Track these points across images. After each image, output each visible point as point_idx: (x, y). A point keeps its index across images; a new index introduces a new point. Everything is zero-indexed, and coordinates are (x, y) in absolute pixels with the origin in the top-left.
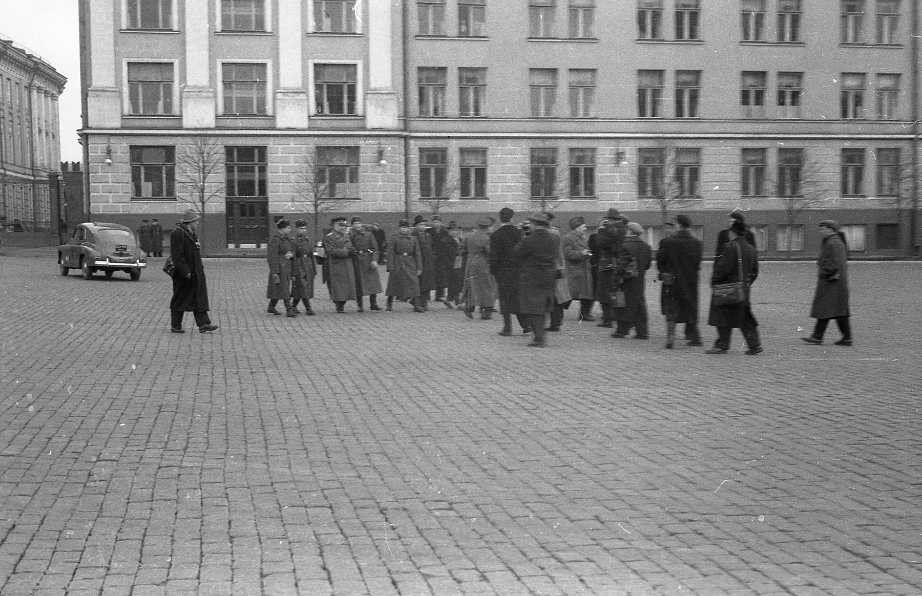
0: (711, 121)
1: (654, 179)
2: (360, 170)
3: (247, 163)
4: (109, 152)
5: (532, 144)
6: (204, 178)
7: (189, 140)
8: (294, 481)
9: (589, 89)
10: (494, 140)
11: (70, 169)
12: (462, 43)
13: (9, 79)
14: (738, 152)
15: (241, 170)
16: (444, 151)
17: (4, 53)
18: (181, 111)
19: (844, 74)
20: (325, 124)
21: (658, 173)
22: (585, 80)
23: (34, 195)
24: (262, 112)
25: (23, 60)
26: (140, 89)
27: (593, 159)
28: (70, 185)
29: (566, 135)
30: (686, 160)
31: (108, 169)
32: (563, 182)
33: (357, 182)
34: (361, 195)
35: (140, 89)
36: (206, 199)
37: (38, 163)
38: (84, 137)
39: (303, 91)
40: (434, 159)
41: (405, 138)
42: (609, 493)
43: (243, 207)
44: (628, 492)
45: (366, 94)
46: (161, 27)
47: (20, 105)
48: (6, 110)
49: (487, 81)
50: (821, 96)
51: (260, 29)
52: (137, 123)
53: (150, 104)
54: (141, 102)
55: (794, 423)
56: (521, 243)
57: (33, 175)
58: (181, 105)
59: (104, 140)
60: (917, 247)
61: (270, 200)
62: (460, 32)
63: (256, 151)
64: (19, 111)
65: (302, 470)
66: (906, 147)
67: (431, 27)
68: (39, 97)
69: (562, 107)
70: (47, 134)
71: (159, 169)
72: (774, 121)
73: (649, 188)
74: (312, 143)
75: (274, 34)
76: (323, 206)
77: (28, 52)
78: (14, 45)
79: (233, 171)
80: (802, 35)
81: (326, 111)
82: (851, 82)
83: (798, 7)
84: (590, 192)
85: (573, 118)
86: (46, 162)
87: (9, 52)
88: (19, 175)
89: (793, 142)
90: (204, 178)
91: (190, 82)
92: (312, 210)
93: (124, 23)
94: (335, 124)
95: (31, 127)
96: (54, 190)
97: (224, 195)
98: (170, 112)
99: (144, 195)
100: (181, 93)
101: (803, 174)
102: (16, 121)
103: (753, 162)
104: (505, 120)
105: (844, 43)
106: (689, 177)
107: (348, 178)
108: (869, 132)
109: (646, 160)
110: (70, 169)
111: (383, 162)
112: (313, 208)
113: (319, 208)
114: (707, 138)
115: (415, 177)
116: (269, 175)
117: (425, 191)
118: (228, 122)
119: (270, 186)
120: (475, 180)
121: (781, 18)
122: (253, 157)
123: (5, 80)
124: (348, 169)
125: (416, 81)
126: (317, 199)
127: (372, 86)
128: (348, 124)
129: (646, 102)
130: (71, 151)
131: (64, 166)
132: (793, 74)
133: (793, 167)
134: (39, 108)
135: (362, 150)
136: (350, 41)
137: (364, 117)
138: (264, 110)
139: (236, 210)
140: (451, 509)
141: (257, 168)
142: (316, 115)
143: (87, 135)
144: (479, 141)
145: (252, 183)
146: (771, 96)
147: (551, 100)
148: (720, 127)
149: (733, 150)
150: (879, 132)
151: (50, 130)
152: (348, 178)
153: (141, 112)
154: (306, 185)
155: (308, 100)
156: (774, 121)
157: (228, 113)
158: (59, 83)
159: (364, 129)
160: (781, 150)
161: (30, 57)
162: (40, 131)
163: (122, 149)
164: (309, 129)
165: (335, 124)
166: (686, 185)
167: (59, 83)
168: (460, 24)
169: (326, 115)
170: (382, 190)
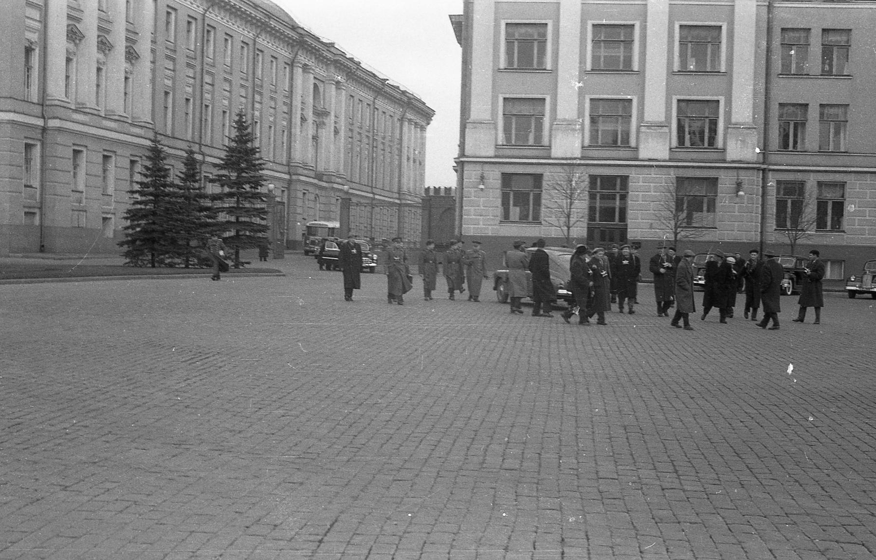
7: (559, 169)
11: (432, 194)
12: (825, 82)
13: (384, 113)
15: (603, 197)
16: (802, 184)
18: (550, 141)
23: (399, 219)
25: (398, 96)
26: (514, 121)
28: (441, 206)
34: (717, 224)
35: (514, 121)
36: (571, 223)
37: (405, 189)
38: (460, 166)
39: (666, 125)
41: (764, 170)
43: (603, 233)
45: (726, 128)
46: (535, 66)
51: (627, 68)
52: (508, 152)
54: (513, 132)
58: (550, 136)
61: (629, 226)
62: (823, 70)
63: (619, 181)
67: (794, 66)
68: (410, 130)
70: (414, 161)
74: (673, 173)
75: (641, 73)
76: (683, 233)
86: (411, 185)
88: (386, 199)
89: (690, 170)
90: (571, 205)
91: (560, 116)
92: (672, 237)
93: (502, 64)
94: (694, 156)
95: (400, 156)
97: (586, 221)
98: (540, 142)
99: (512, 219)
100: (551, 125)
102: (388, 150)
107: (705, 208)
110: (432, 194)
111: (741, 193)
112: (673, 235)
113: (679, 236)
115: (772, 210)
117: (781, 224)
119: (630, 213)
122: (615, 185)
123: (381, 113)
124: (706, 200)
126: (676, 227)
127: (733, 120)
131: (427, 190)
134: (409, 140)
135: (720, 181)
136: (715, 80)
137: (724, 150)
138: (628, 142)
139: (597, 235)
142: (677, 148)
144: (837, 175)
145: (614, 209)
152: (705, 208)
153: (513, 142)
154: (668, 214)
155: (670, 132)
157: (594, 144)
158: (427, 114)
159: (724, 161)
161: (404, 93)
162: (408, 159)
163: (494, 177)
164: (670, 160)
165: (694, 156)
168: (823, 63)
169: (687, 148)
170: (738, 222)
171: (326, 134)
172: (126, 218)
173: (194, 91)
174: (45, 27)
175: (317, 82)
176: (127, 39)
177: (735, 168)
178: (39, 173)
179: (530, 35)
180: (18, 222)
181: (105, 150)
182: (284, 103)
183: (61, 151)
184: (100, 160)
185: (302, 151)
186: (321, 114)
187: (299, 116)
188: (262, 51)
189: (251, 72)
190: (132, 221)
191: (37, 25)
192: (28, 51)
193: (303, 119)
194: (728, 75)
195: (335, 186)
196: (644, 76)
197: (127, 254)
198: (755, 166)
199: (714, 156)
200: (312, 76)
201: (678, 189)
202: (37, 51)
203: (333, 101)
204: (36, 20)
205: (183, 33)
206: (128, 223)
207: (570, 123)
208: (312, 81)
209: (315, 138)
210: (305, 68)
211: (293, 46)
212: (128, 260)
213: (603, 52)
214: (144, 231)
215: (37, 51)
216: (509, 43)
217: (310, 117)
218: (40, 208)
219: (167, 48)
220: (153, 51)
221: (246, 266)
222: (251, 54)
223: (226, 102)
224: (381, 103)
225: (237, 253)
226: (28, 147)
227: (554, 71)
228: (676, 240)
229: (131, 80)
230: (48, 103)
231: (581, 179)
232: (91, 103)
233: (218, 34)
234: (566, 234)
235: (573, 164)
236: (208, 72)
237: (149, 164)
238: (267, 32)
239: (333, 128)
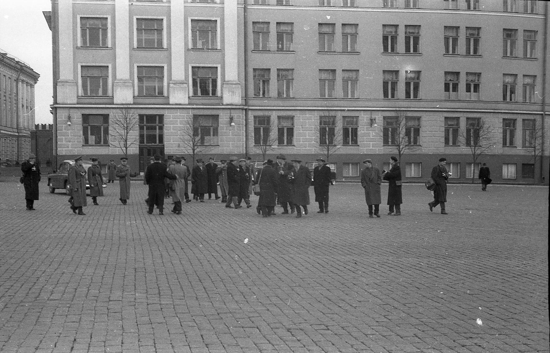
0: (427, 101)
1: (392, 135)
2: (219, 129)
3: (152, 124)
4: (69, 118)
5: (322, 114)
6: (127, 133)
7: (118, 110)
8: (231, 313)
9: (355, 81)
10: (340, 112)
14: (443, 119)
15: (148, 128)
16: (269, 118)
17: (2, 61)
19: (504, 75)
20: (198, 102)
21: (395, 131)
22: (352, 76)
23: (18, 144)
24: (161, 93)
27: (357, 123)
28: (43, 136)
29: (342, 108)
30: (411, 123)
31: (69, 127)
32: (339, 137)
33: (217, 135)
34: (220, 143)
37: (21, 125)
38: (54, 110)
40: (263, 122)
41: (246, 110)
42: (418, 321)
43: (149, 151)
44: (429, 320)
45: (222, 84)
46: (101, 46)
47: (11, 90)
48: (3, 94)
49: (294, 76)
50: (491, 88)
51: (160, 46)
53: (95, 90)
55: (510, 280)
56: (312, 173)
57: (18, 133)
58: (113, 90)
60: (544, 178)
64: (10, 95)
65: (234, 306)
66: (538, 118)
69: (339, 91)
71: (99, 128)
72: (464, 101)
73: (390, 140)
74: (191, 113)
75: (169, 49)
76: (198, 150)
77: (16, 60)
78: (8, 56)
79: (143, 129)
80: (480, 52)
81: (199, 93)
82: (509, 80)
83: (478, 34)
84: (355, 142)
85: (345, 98)
86: (26, 124)
87: (5, 60)
90: (127, 133)
91: (118, 77)
92: (191, 152)
95: (17, 104)
96: (34, 141)
97: (138, 143)
101: (481, 133)
103: (452, 125)
104: (302, 99)
105: (505, 56)
106: (414, 133)
107: (212, 133)
108: (519, 109)
109: (388, 123)
111: (233, 124)
112: (192, 151)
113: (196, 151)
114: (424, 111)
116: (165, 131)
117: (257, 142)
118: (140, 100)
120: (287, 134)
121: (468, 40)
124: (212, 128)
125: (252, 77)
126: (194, 146)
128: (212, 101)
129: (389, 88)
130: (43, 116)
131: (37, 126)
132: (475, 74)
133: (475, 130)
134: (23, 93)
137: (222, 97)
139: (145, 152)
140: (328, 329)
141: (157, 127)
143: (56, 108)
145: (155, 136)
146: (462, 86)
147: (332, 88)
148: (489, 106)
149: (441, 118)
150: (524, 109)
151: (29, 105)
152: (212, 133)
154: (187, 137)
156: (464, 101)
160: (468, 119)
161: (18, 62)
162: (23, 106)
163: (77, 117)
164: (189, 104)
166: (412, 140)
167: (34, 77)
170: (231, 141)
198: (240, 107)
199: (217, 101)
213: (144, 36)
228: (194, 154)
234: (125, 152)
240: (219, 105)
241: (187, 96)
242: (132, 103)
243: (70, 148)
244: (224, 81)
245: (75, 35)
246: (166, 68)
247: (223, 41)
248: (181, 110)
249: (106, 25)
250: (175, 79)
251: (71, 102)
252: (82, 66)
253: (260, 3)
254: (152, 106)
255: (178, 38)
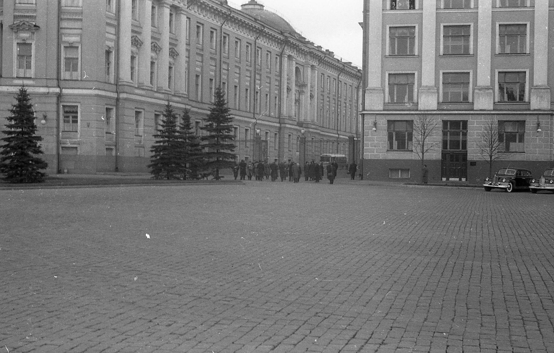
3: (456, 129)
4: (375, 124)
17: (343, 69)
24: (466, 98)
43: (452, 156)
46: (408, 53)
51: (466, 53)
52: (391, 107)
59: (535, 117)
74: (496, 119)
75: (475, 55)
78: (352, 65)
91: (424, 83)
94: (508, 107)
111: (539, 130)
113: (493, 158)
116: (469, 137)
119: (469, 144)
124: (518, 134)
142: (498, 102)
145: (459, 141)
159: (529, 110)
163: (383, 122)
164: (494, 110)
171: (305, 98)
172: (152, 151)
173: (215, 74)
174: (118, 38)
175: (297, 65)
176: (170, 44)
177: (536, 114)
178: (114, 125)
179: (404, 34)
180: (102, 155)
181: (156, 111)
182: (276, 80)
183: (127, 112)
184: (153, 117)
185: (288, 108)
186: (301, 86)
187: (285, 87)
188: (261, 48)
189: (253, 62)
190: (156, 152)
191: (114, 37)
192: (108, 53)
193: (289, 89)
194: (531, 55)
195: (311, 130)
196: (533, 57)
197: (152, 172)
198: (549, 112)
199: (524, 107)
200: (294, 62)
201: (389, 127)
202: (114, 52)
203: (309, 77)
204: (112, 34)
205: (207, 38)
206: (154, 153)
207: (429, 88)
208: (294, 66)
209: (298, 101)
210: (290, 57)
211: (281, 44)
212: (153, 176)
213: (450, 43)
214: (162, 158)
215: (114, 52)
216: (392, 38)
217: (294, 88)
218: (116, 146)
219: (197, 48)
220: (188, 50)
221: (222, 178)
222: (253, 50)
223: (237, 81)
224: (342, 77)
225: (217, 171)
226: (108, 110)
227: (420, 56)
228: (491, 161)
229: (173, 69)
230: (120, 83)
231: (438, 122)
232: (147, 82)
233: (231, 39)
234: (421, 157)
235: (426, 114)
236: (225, 63)
237: (165, 119)
238: (263, 36)
239: (309, 94)
240: (526, 110)
241: (492, 102)
242: (436, 109)
243: (375, 153)
244: (533, 86)
245: (383, 45)
246: (527, 74)
247: (532, 45)
248: (485, 116)
249: (414, 33)
250: (481, 84)
251: (378, 109)
252: (499, 72)
253: (507, 5)
254: (456, 112)
255: (484, 44)
